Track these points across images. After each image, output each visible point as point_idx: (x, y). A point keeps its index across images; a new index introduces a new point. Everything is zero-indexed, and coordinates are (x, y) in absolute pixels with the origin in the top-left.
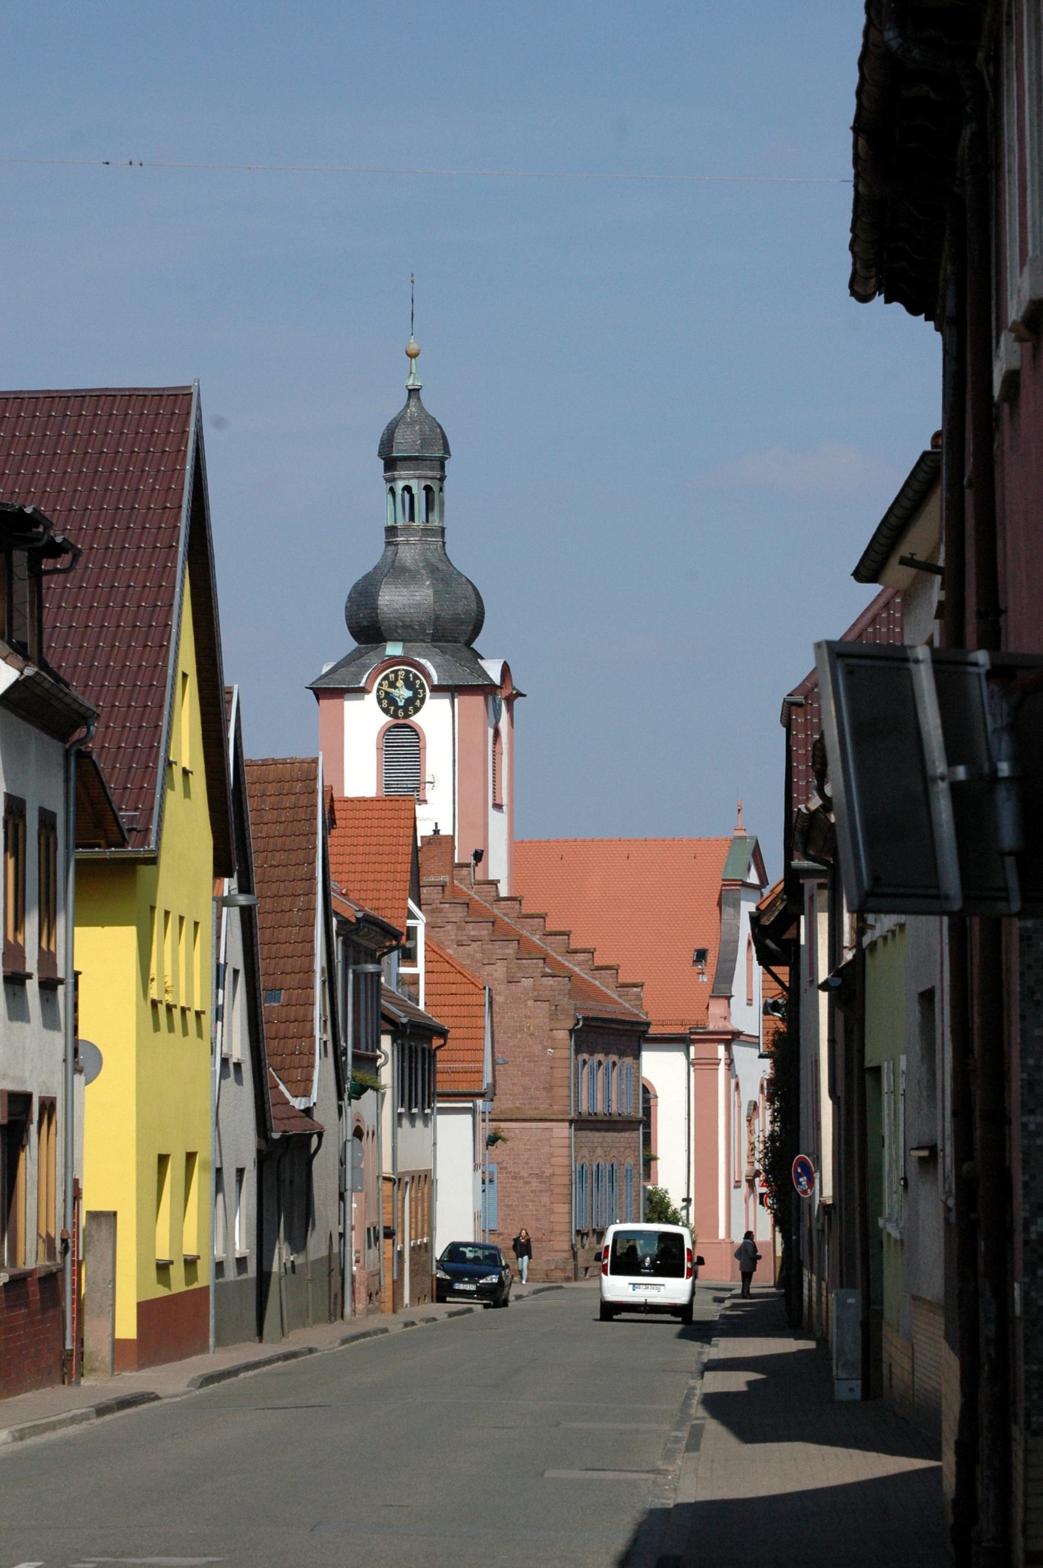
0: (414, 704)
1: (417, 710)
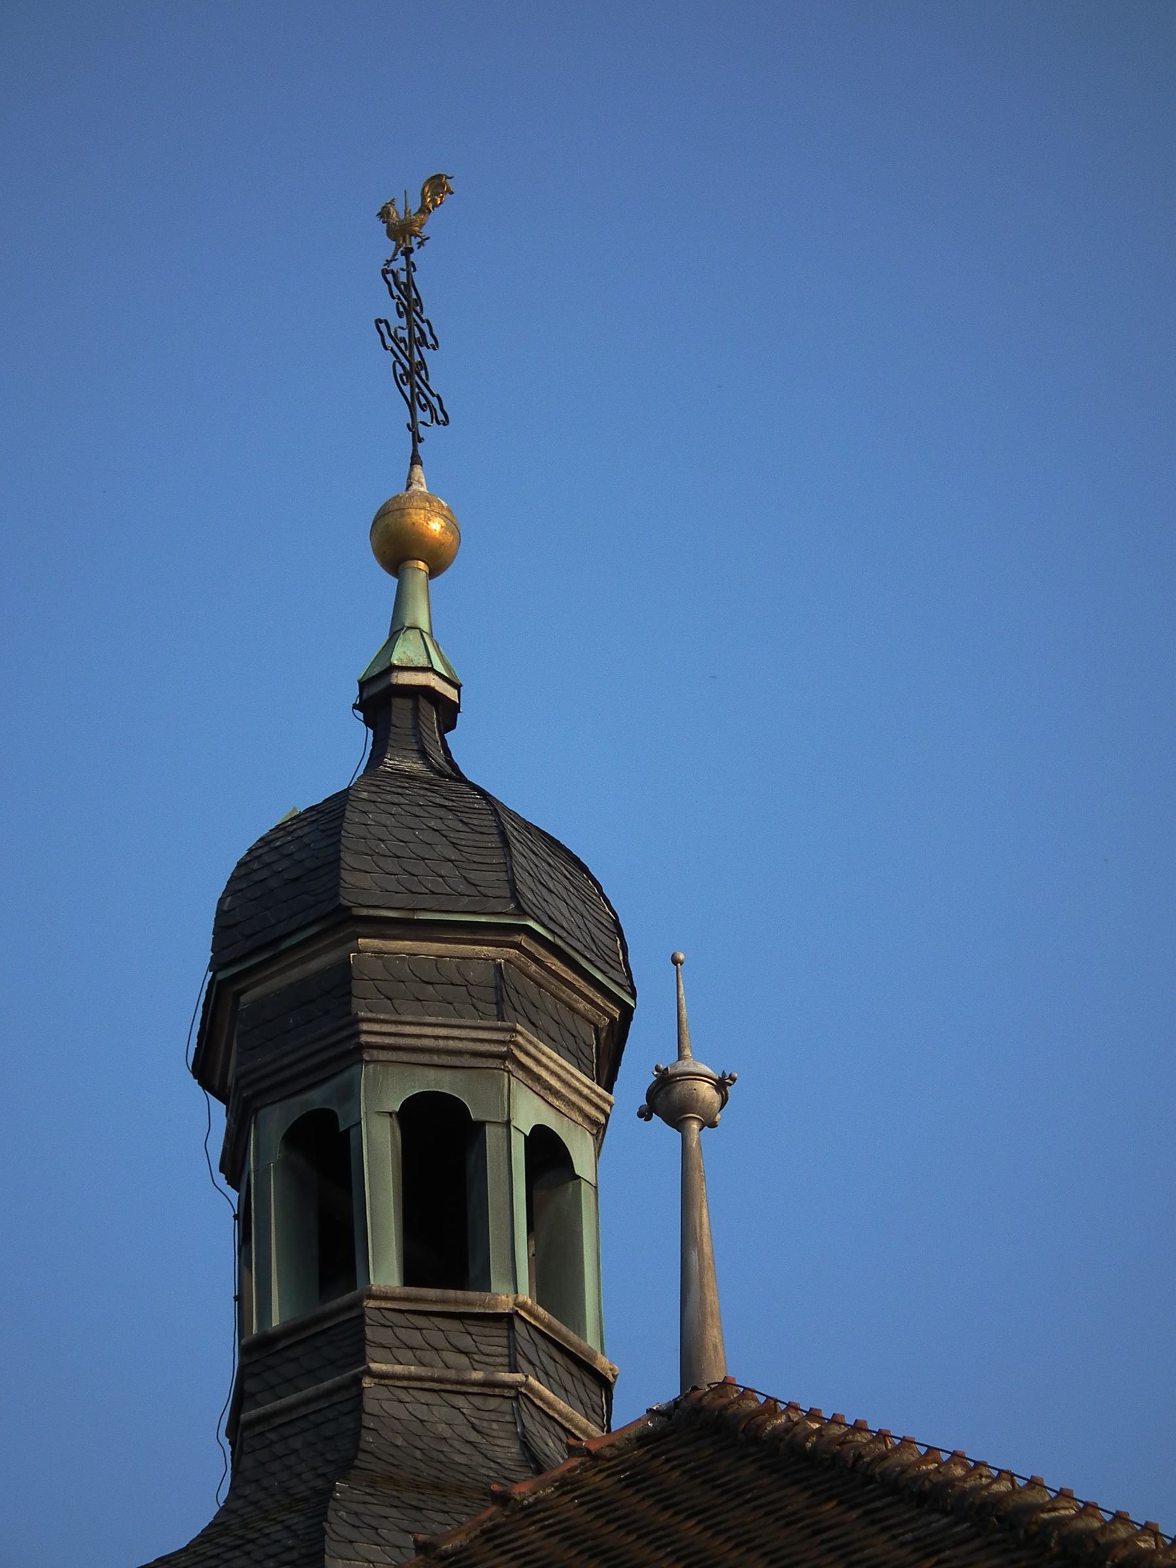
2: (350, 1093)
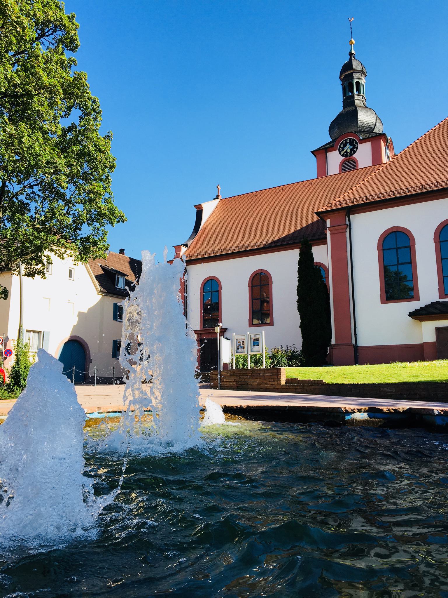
0: (354, 150)
1: (355, 152)
2: (353, 81)
